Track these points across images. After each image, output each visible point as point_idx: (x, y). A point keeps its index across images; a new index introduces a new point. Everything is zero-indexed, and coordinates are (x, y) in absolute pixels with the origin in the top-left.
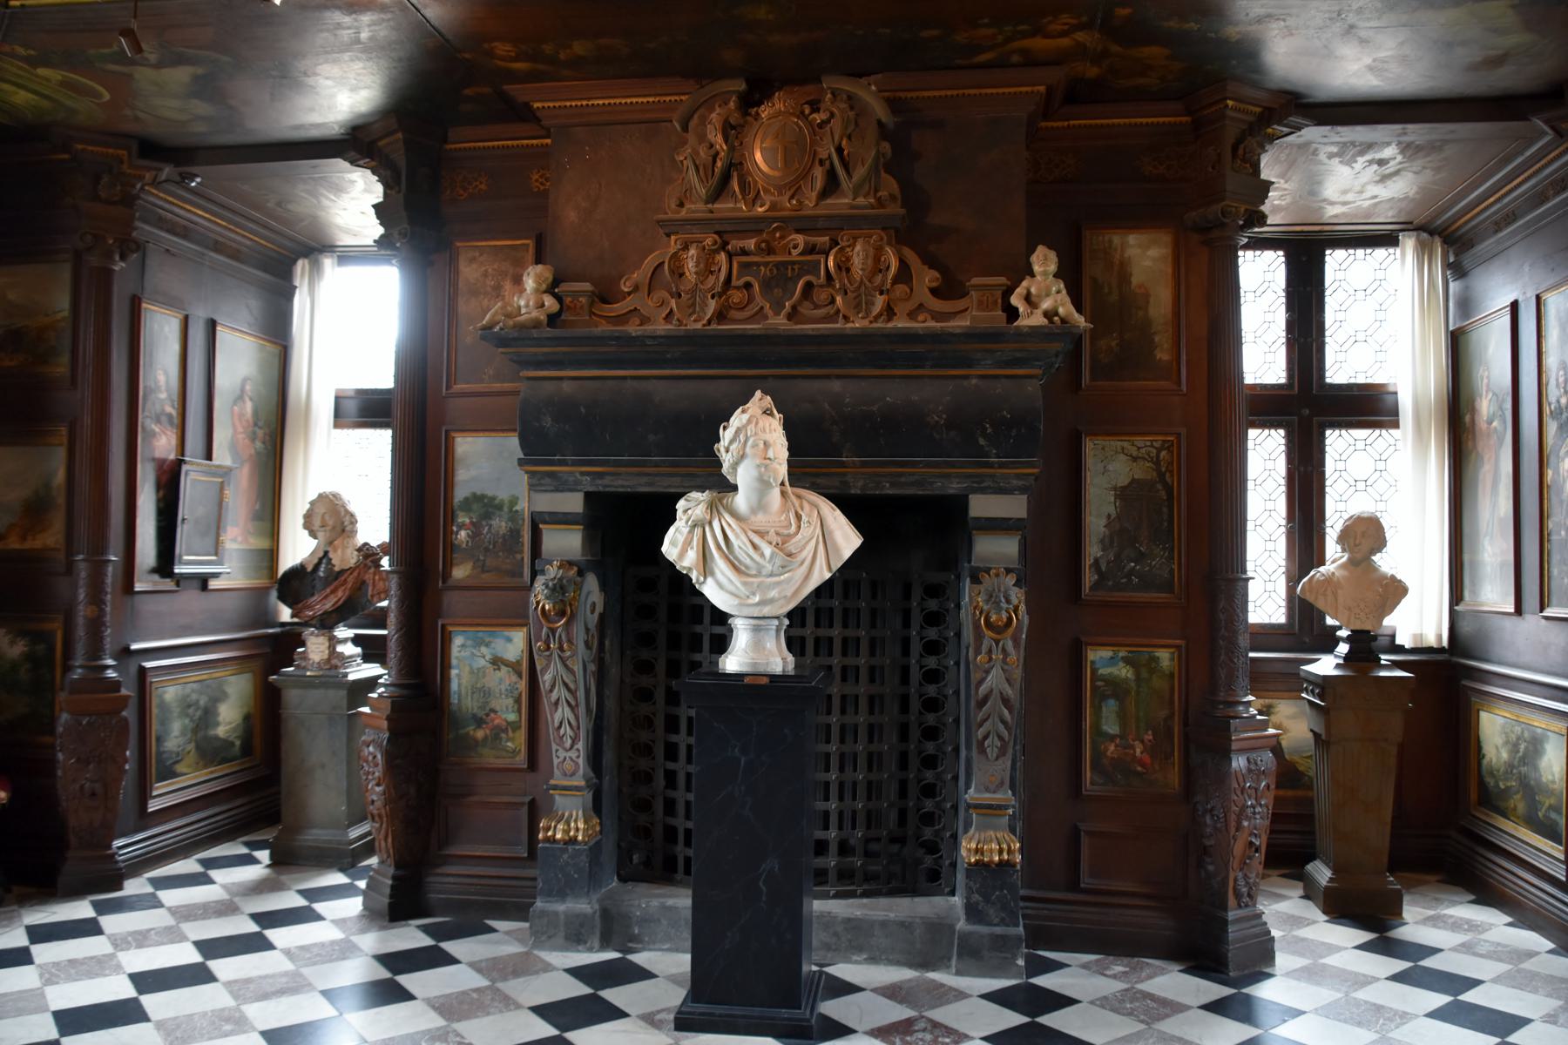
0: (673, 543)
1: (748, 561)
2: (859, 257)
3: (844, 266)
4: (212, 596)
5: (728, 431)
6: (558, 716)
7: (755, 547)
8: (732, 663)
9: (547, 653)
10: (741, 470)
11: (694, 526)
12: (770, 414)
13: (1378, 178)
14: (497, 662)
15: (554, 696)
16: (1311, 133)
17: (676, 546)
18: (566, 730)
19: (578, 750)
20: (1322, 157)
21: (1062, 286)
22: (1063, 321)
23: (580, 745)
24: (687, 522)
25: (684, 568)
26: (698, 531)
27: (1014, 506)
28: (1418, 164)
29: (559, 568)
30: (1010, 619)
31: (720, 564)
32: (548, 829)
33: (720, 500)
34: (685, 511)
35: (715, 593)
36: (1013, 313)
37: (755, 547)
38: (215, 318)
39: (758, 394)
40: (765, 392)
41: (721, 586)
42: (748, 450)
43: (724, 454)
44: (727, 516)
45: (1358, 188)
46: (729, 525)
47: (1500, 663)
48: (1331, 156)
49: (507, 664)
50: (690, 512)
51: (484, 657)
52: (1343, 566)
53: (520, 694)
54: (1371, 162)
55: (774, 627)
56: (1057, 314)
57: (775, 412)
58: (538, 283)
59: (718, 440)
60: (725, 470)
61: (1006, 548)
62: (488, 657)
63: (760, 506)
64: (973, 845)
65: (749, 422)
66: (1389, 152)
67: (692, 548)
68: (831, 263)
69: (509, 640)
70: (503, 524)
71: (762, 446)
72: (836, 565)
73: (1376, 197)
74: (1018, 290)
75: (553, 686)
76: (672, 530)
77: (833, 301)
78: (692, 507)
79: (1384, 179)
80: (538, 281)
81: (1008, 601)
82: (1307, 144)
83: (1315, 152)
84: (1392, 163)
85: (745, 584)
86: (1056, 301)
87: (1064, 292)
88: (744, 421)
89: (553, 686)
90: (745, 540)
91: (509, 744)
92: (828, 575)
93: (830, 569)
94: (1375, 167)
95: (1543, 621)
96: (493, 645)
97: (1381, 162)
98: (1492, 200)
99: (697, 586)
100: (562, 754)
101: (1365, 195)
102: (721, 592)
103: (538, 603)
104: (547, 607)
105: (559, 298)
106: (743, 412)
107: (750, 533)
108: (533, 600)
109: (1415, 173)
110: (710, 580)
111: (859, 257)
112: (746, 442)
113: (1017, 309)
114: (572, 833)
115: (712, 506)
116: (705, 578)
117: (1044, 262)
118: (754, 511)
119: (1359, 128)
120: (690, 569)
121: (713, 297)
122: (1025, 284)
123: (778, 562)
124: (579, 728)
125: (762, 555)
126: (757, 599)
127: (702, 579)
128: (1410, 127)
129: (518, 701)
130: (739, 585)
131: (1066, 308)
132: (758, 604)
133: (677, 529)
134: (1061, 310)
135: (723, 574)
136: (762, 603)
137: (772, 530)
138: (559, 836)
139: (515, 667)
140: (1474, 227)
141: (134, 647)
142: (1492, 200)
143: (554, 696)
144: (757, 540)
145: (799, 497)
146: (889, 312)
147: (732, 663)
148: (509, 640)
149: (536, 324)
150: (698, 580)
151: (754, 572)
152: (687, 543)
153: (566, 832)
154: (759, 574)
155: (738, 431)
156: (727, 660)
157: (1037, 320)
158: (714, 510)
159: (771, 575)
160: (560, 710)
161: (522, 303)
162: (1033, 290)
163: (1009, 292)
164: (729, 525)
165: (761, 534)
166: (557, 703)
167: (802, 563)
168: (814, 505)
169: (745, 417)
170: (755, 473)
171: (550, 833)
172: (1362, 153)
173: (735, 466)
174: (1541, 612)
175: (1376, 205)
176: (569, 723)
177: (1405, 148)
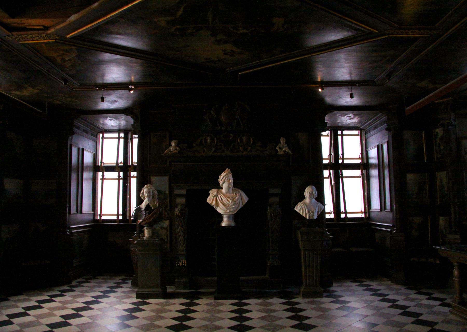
0: (210, 200)
1: (226, 203)
2: (244, 139)
3: (241, 140)
4: (83, 214)
5: (221, 177)
6: (180, 238)
7: (228, 200)
8: (223, 224)
9: (179, 225)
10: (224, 185)
11: (214, 197)
12: (230, 173)
13: (349, 119)
14: (162, 228)
15: (179, 234)
16: (335, 112)
17: (210, 200)
18: (182, 242)
19: (184, 246)
20: (337, 115)
21: (287, 145)
22: (287, 153)
23: (185, 245)
24: (213, 196)
25: (212, 205)
26: (215, 198)
27: (277, 191)
28: (357, 117)
29: (181, 206)
30: (278, 214)
31: (220, 204)
32: (178, 263)
33: (219, 191)
34: (212, 193)
35: (220, 210)
36: (277, 151)
37: (228, 200)
38: (84, 148)
39: (227, 169)
40: (229, 169)
41: (221, 209)
42: (226, 180)
43: (220, 181)
44: (222, 195)
45: (345, 120)
46: (222, 196)
47: (373, 221)
48: (339, 115)
49: (164, 228)
50: (213, 193)
51: (159, 227)
52: (108, 118)
53: (168, 235)
54: (348, 116)
55: (232, 217)
56: (286, 151)
57: (231, 173)
58: (175, 144)
59: (219, 178)
60: (221, 184)
61: (276, 200)
62: (160, 227)
63: (228, 192)
64: (271, 262)
65: (226, 175)
66: (350, 115)
67: (214, 201)
68: (239, 140)
69: (164, 223)
70: (163, 197)
71: (228, 179)
72: (244, 204)
73: (349, 122)
74: (278, 146)
75: (179, 232)
76: (209, 197)
77: (239, 148)
78: (213, 192)
79: (350, 119)
80: (175, 143)
81: (278, 210)
82: (335, 114)
83: (336, 115)
84: (352, 117)
85: (226, 208)
86: (286, 149)
87: (287, 147)
88: (225, 175)
89: (179, 232)
90: (226, 199)
91: (165, 246)
92: (242, 206)
93: (243, 204)
94: (348, 117)
95: (386, 212)
96: (161, 224)
97: (350, 117)
98: (373, 123)
99: (215, 209)
100: (181, 247)
101: (347, 122)
102: (221, 210)
103: (177, 214)
104: (179, 214)
105: (180, 147)
106: (224, 173)
107: (226, 198)
108: (175, 213)
109: (357, 118)
110: (218, 207)
111: (244, 139)
112: (225, 179)
113: (278, 150)
114: (184, 264)
115: (217, 192)
116: (217, 207)
117: (282, 141)
118: (227, 193)
119: (344, 111)
120: (214, 205)
121: (213, 147)
122: (279, 145)
123: (233, 203)
124: (185, 241)
125: (229, 202)
126: (229, 211)
127: (216, 207)
128: (354, 111)
129: (167, 237)
130: (225, 208)
131: (288, 150)
132: (229, 212)
133: (210, 197)
134: (287, 151)
135: (221, 206)
136: (230, 212)
137: (231, 197)
138: (181, 265)
139: (166, 229)
140: (373, 117)
141: (71, 227)
142: (373, 123)
143: (179, 234)
144: (228, 199)
145: (235, 190)
146: (251, 151)
147: (223, 224)
148: (164, 223)
149: (176, 153)
150: (216, 208)
151: (228, 205)
152: (213, 200)
153: (182, 263)
154: (229, 206)
155: (224, 177)
156: (222, 224)
157: (282, 153)
158: (218, 193)
159: (231, 206)
160: (180, 237)
161: (171, 148)
162: (281, 146)
163: (276, 147)
164: (222, 196)
165: (229, 198)
166: (180, 236)
167: (237, 203)
168: (239, 192)
169: (225, 174)
170: (227, 185)
171: (179, 265)
172: (345, 115)
173: (223, 184)
174: (385, 210)
175: (350, 123)
176: (183, 240)
177: (354, 115)
